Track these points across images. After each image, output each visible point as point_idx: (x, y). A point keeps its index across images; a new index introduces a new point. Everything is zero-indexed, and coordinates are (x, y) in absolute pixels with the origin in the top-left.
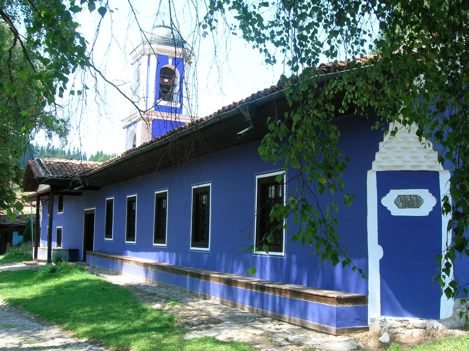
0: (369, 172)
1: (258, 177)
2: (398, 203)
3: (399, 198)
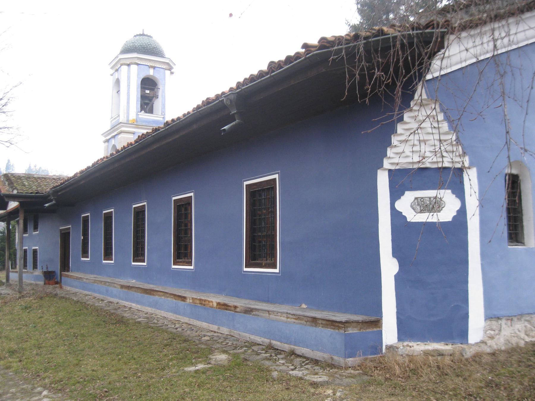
0: (379, 172)
1: (246, 183)
2: (414, 207)
3: (416, 201)
